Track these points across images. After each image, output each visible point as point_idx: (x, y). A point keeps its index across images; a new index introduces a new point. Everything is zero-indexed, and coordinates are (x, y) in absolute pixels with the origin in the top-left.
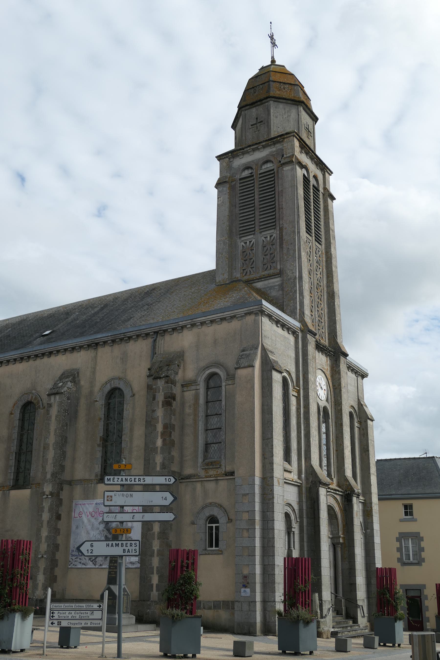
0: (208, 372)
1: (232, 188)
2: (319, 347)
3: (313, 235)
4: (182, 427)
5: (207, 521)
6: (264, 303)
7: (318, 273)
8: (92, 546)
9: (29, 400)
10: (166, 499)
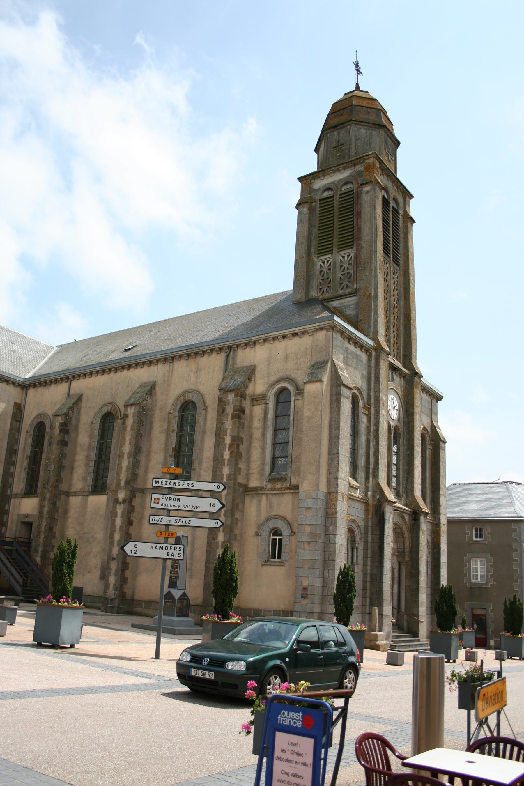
0: (277, 387)
1: (311, 210)
3: (391, 256)
4: (250, 441)
5: (270, 533)
6: (336, 318)
8: (136, 546)
9: (109, 410)
10: (214, 505)
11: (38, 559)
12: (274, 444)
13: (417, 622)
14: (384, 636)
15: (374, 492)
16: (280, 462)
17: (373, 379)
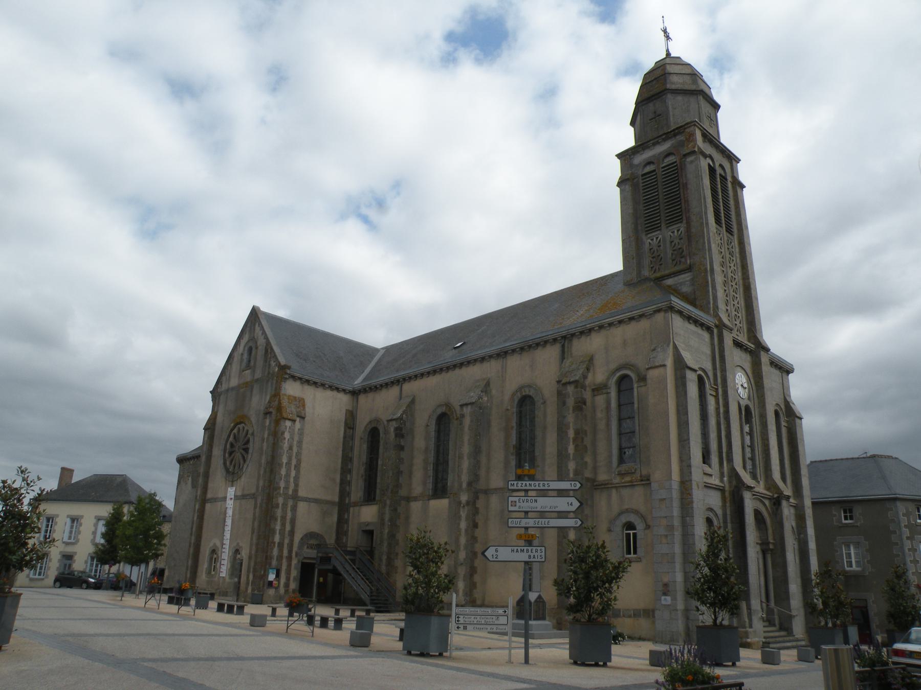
0: (618, 375)
1: (635, 187)
2: (738, 344)
6: (673, 298)
7: (732, 265)
8: (496, 551)
10: (571, 504)
11: (384, 569)
12: (620, 434)
13: (791, 618)
14: (758, 630)
15: (730, 477)
16: (629, 452)
17: (719, 357)
